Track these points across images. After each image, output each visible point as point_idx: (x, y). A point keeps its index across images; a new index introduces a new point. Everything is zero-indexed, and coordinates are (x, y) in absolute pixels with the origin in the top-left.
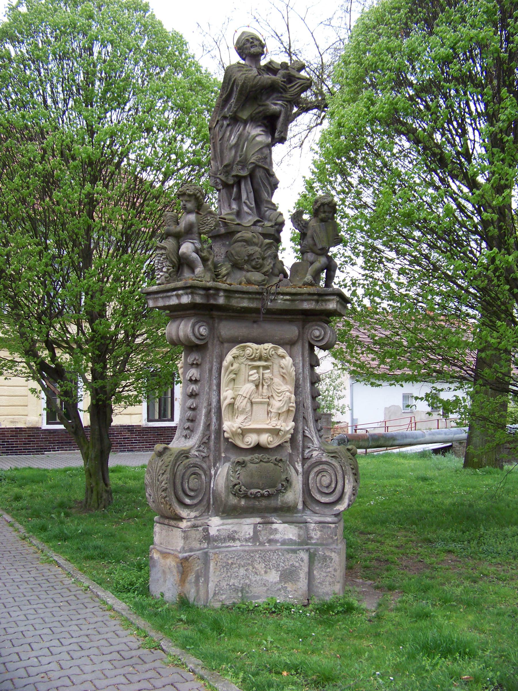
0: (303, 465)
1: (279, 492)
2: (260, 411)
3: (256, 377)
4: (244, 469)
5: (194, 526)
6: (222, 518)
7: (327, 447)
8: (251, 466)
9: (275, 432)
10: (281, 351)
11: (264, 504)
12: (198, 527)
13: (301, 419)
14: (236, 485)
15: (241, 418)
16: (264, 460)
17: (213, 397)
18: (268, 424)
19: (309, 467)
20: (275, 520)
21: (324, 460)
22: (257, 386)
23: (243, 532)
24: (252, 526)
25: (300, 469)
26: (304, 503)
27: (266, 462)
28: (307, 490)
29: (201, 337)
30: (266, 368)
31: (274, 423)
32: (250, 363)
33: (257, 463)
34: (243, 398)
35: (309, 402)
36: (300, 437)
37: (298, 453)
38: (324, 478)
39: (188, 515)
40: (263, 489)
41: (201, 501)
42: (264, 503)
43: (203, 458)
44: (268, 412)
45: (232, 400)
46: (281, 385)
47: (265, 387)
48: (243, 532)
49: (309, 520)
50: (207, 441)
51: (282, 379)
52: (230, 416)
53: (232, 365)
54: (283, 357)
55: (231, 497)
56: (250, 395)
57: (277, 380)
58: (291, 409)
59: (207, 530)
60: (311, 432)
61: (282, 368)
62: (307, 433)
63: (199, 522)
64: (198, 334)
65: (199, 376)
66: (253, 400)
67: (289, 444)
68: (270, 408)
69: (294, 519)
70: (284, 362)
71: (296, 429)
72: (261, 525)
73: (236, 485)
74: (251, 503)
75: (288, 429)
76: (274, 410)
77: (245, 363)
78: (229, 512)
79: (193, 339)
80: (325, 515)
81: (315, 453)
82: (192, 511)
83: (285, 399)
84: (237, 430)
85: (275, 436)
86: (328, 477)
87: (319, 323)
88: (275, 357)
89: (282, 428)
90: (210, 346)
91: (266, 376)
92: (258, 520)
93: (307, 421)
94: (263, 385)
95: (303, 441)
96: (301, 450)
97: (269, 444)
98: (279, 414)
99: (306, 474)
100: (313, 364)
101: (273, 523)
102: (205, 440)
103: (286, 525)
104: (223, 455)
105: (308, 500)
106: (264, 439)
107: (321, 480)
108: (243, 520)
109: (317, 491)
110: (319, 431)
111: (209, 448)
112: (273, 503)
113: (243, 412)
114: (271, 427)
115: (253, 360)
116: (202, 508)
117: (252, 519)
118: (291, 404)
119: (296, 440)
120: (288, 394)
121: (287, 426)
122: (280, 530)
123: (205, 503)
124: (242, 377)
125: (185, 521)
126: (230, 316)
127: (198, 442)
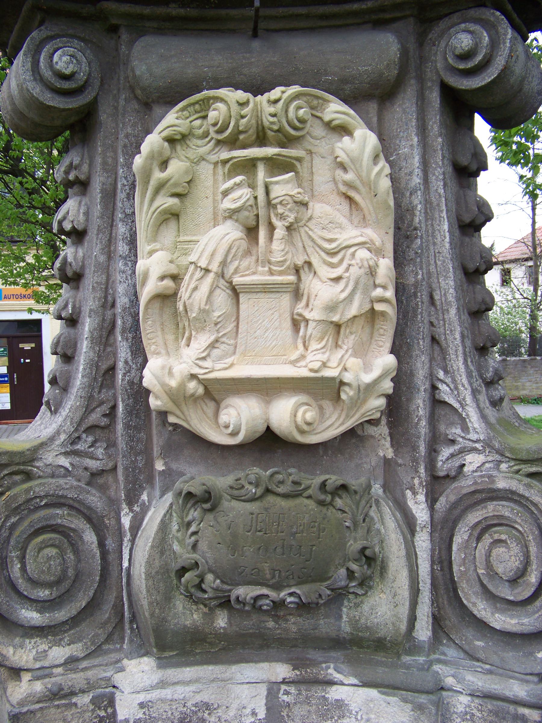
0: (432, 500)
1: (339, 595)
2: (265, 316)
3: (242, 196)
4: (210, 517)
5: (56, 695)
6: (163, 663)
7: (512, 441)
8: (234, 509)
9: (325, 389)
10: (335, 109)
11: (294, 628)
12: (73, 694)
13: (423, 344)
14: (183, 571)
15: (201, 341)
16: (281, 490)
17: (119, 277)
18: (294, 363)
19: (454, 506)
20: (338, 676)
21: (501, 484)
22: (252, 232)
23: (234, 706)
24: (263, 690)
25: (420, 510)
26: (437, 621)
27: (286, 496)
28: (445, 584)
29: (65, 85)
30: (277, 166)
31: (317, 359)
32: (225, 155)
33: (253, 499)
34: (198, 274)
35: (448, 286)
36: (420, 406)
37: (415, 461)
38: (499, 551)
39: (42, 655)
40: (278, 587)
41: (93, 606)
42: (294, 625)
43: (93, 475)
44: (297, 323)
45: (168, 283)
46: (340, 227)
47: (280, 232)
48: (234, 706)
49: (450, 681)
50: (104, 421)
51: (345, 206)
52: (170, 337)
53: (164, 164)
54: (344, 130)
55: (179, 603)
56: (224, 264)
57: (325, 209)
58: (379, 307)
59: (112, 702)
60: (459, 387)
61: (343, 167)
62: (445, 392)
63: (77, 679)
64: (47, 74)
65: (82, 218)
66: (237, 280)
67: (383, 429)
68: (300, 308)
69: (399, 676)
70: (345, 146)
71: (402, 379)
72: (292, 689)
73: (183, 571)
74: (249, 624)
75: (367, 378)
76: (314, 315)
77: (213, 158)
78: (178, 647)
79: (50, 100)
80: (504, 672)
81: (473, 461)
82: (58, 643)
83: (355, 272)
84: (182, 386)
85: (327, 405)
86: (515, 548)
87: (473, 13)
88: (319, 131)
89: (348, 377)
90: (104, 115)
91: (277, 192)
92: (281, 671)
93: (444, 352)
94: (272, 228)
95: (433, 420)
96: (422, 449)
97: (302, 432)
98: (338, 326)
99: (443, 530)
100: (464, 160)
101: (331, 683)
102: (95, 417)
103: (373, 693)
104: (159, 466)
105: (451, 618)
106: (285, 414)
107: (488, 555)
108: (234, 668)
109: (477, 588)
110: (489, 384)
111: (111, 444)
112: (324, 625)
113: (203, 321)
114: (304, 373)
115: (233, 142)
116: (91, 630)
117: (265, 665)
118: (378, 292)
119: (408, 415)
120: (363, 254)
121: (367, 367)
122: (354, 707)
123: (106, 612)
124: (203, 204)
125: (26, 677)
126: (170, 19)
127: (69, 427)
